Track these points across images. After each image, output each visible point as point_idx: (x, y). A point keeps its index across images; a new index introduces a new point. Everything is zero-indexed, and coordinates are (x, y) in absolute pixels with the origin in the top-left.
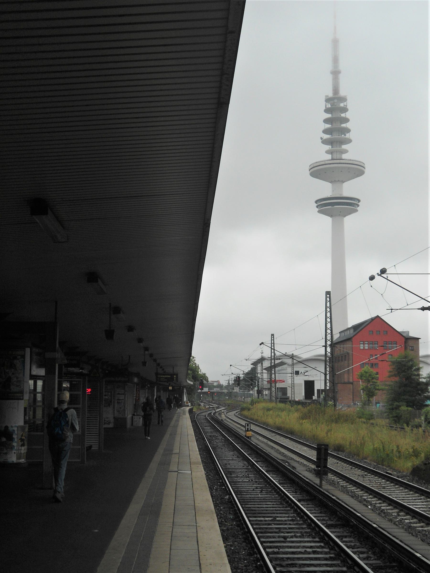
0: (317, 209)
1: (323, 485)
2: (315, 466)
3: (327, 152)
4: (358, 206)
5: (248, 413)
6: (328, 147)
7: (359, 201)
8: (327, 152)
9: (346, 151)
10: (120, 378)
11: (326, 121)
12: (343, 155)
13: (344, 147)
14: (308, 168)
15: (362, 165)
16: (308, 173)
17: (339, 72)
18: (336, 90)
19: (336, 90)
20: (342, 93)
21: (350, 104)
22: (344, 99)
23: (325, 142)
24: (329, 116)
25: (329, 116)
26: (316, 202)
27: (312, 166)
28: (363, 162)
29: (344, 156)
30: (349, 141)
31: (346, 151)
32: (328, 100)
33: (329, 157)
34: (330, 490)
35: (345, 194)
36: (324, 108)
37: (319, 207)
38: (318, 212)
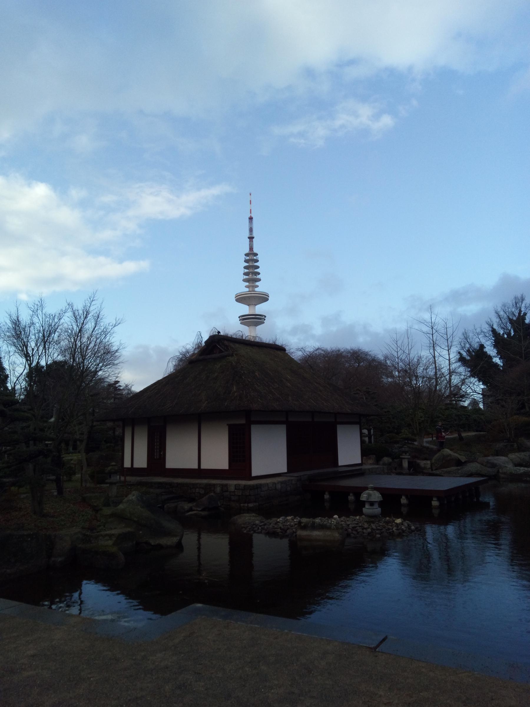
0: (240, 322)
1: (56, 491)
2: (124, 393)
3: (246, 287)
4: (265, 320)
5: (398, 445)
6: (247, 284)
7: (265, 317)
8: (246, 287)
9: (257, 286)
10: (32, 533)
11: (245, 268)
12: (256, 288)
13: (257, 284)
14: (234, 296)
15: (267, 294)
16: (235, 299)
17: (253, 238)
18: (251, 249)
19: (251, 249)
20: (255, 251)
21: (259, 257)
22: (256, 255)
23: (245, 280)
24: (247, 264)
25: (247, 264)
26: (239, 317)
27: (236, 296)
28: (267, 293)
29: (256, 289)
30: (259, 280)
31: (257, 286)
32: (247, 255)
33: (247, 290)
34: (123, 361)
35: (257, 313)
36: (244, 260)
37: (241, 320)
38: (241, 323)
